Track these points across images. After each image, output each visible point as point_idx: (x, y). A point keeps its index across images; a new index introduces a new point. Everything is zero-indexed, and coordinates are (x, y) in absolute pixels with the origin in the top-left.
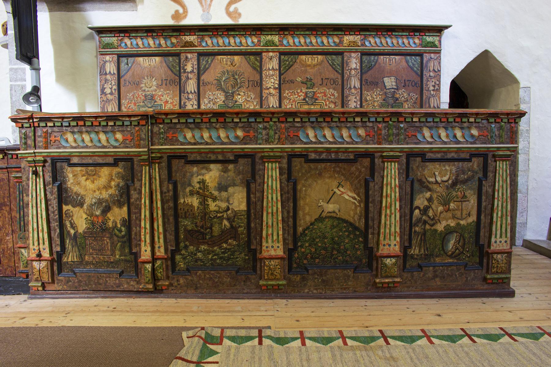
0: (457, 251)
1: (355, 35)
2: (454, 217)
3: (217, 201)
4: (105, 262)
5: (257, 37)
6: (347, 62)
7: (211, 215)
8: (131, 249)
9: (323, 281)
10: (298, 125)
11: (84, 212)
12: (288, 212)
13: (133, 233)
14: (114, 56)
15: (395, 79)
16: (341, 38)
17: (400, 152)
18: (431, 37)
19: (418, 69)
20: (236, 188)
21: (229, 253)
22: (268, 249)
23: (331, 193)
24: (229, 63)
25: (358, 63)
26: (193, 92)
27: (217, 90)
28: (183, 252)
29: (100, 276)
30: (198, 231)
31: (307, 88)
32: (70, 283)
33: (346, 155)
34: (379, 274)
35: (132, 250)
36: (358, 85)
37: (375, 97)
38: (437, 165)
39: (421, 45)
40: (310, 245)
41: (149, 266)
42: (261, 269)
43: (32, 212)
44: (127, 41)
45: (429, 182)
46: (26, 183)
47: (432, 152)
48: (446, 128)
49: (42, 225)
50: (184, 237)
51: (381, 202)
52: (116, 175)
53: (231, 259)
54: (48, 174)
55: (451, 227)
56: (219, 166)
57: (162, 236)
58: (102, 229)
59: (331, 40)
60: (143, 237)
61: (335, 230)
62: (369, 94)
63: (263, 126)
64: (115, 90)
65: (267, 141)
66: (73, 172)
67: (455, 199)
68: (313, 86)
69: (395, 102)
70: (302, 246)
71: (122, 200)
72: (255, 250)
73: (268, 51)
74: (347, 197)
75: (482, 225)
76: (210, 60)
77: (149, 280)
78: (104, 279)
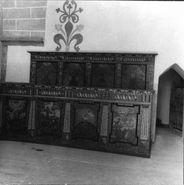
0: (129, 138)
2: (128, 126)
38: (122, 108)
45: (119, 113)
47: (120, 103)
73: (88, 62)
74: (91, 116)
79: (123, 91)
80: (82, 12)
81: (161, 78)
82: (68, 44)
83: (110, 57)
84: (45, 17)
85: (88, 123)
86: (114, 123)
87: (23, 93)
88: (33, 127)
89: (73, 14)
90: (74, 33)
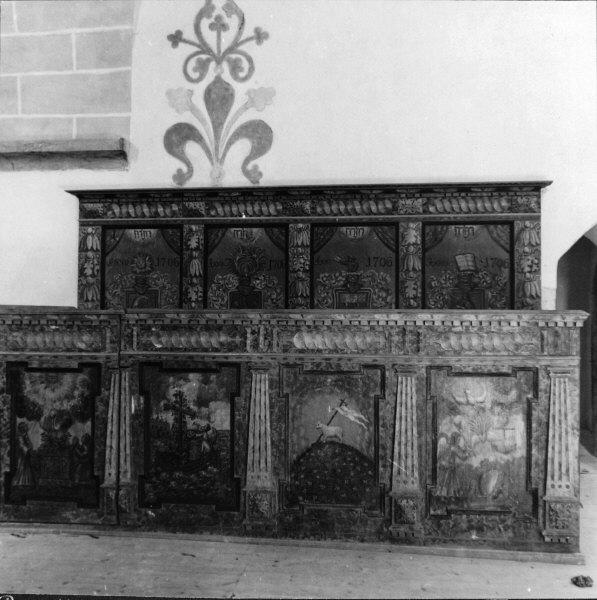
9: (322, 524)
20: (218, 402)
36: (418, 266)
41: (112, 494)
71: (86, 412)
73: (296, 221)
76: (220, 235)
79: (298, 317)
80: (265, 42)
82: (216, 157)
83: (377, 200)
84: (130, 65)
85: (341, 448)
86: (442, 441)
88: (126, 472)
89: (231, 50)
90: (238, 115)
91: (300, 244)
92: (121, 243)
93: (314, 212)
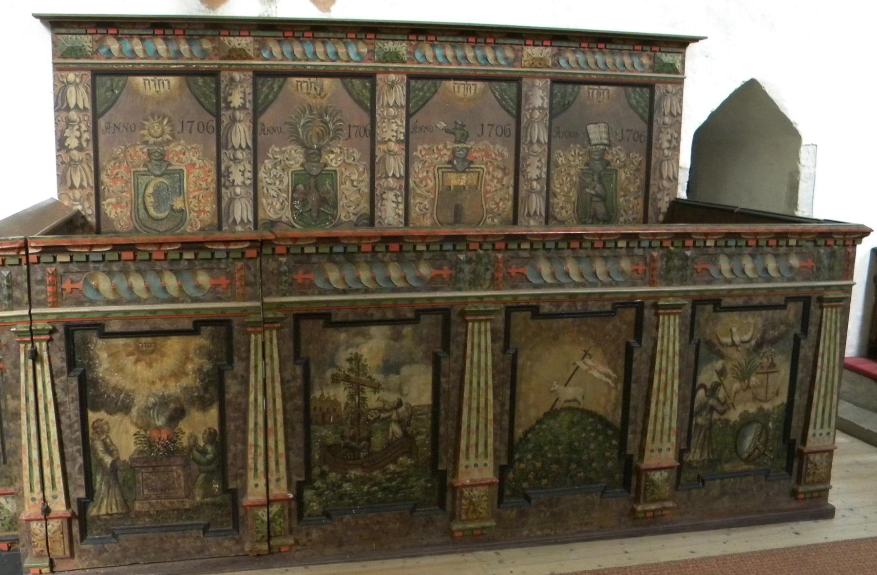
0: (757, 451)
1: (543, 45)
2: (755, 398)
3: (381, 392)
4: (174, 510)
5: (366, 44)
6: (526, 94)
7: (369, 417)
8: (224, 482)
10: (525, 254)
11: (132, 422)
12: (502, 405)
13: (230, 455)
14: (84, 72)
15: (605, 127)
16: (518, 50)
17: (683, 297)
18: (669, 55)
19: (645, 111)
21: (399, 480)
22: (469, 469)
23: (573, 368)
24: (313, 92)
25: (545, 98)
26: (244, 146)
27: (290, 142)
28: (318, 484)
29: (166, 536)
30: (346, 446)
31: (456, 142)
32: (106, 554)
33: (599, 303)
34: (642, 497)
35: (228, 485)
36: (544, 138)
37: (571, 159)
38: (735, 315)
39: (653, 69)
40: (534, 457)
42: (453, 503)
43: (29, 429)
44: (114, 45)
45: (723, 345)
46: (12, 374)
48: (753, 256)
49: (50, 453)
50: (320, 457)
51: (651, 381)
52: (195, 350)
53: (402, 489)
54: (59, 354)
55: (749, 414)
56: (385, 329)
57: (282, 461)
58: (169, 451)
59: (499, 54)
60: (250, 462)
61: (574, 430)
62: (562, 154)
63: (466, 256)
64: (87, 141)
65: (474, 284)
66: (108, 348)
67: (759, 370)
68: (465, 138)
69: (605, 169)
70: (520, 460)
71: (207, 396)
72: (444, 473)
73: (387, 71)
75: (795, 410)
76: (276, 87)
77: (263, 537)
78: (173, 542)
81: (700, 136)
87: (190, 290)
91: (391, 104)
92: (121, 98)
93: (413, 60)
